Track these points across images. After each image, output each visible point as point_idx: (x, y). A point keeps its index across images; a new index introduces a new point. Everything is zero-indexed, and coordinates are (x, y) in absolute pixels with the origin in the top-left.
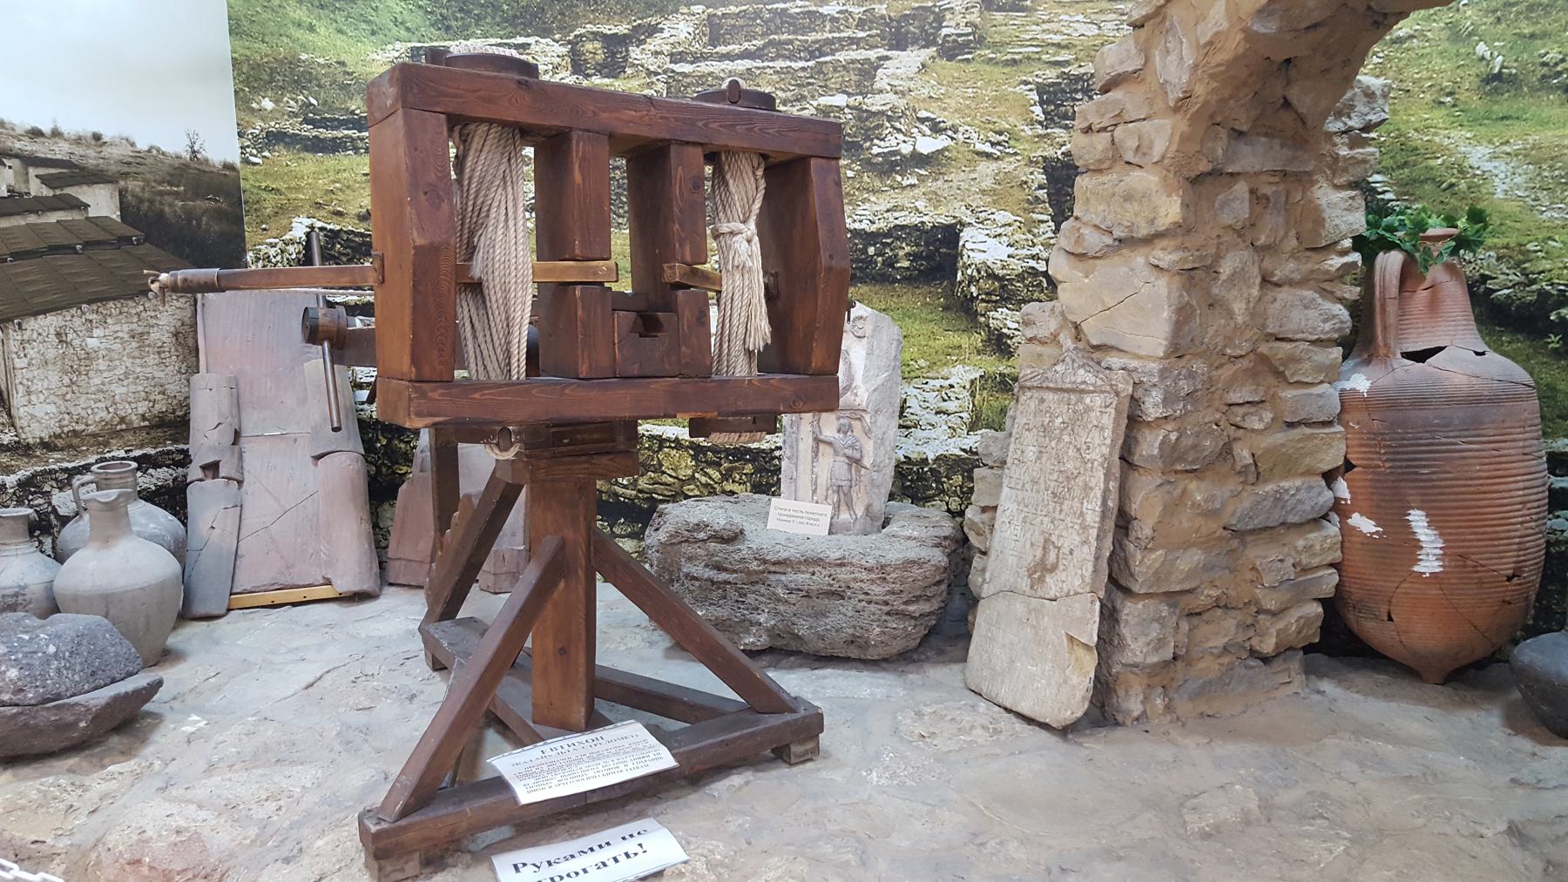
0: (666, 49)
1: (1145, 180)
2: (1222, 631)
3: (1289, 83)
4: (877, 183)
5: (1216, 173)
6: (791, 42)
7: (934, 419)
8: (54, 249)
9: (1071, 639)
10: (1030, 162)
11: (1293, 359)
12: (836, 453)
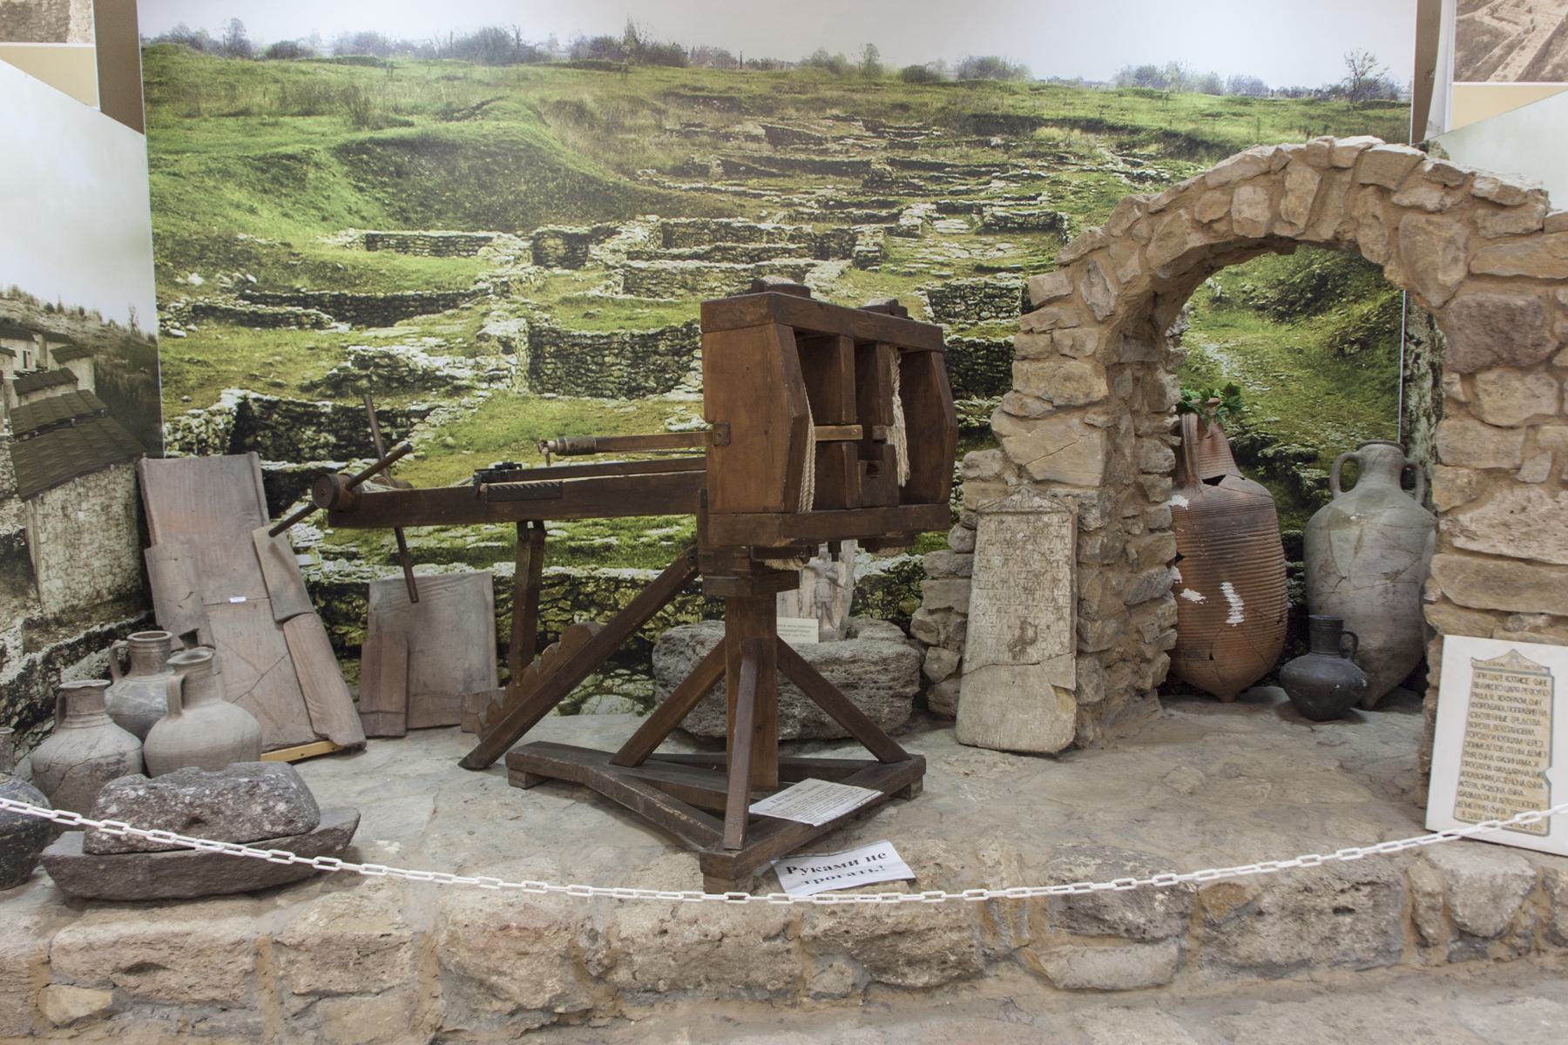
0: (624, 248)
2: (1125, 677)
6: (734, 249)
8: (63, 422)
9: (1055, 688)
11: (1153, 486)
12: (818, 575)
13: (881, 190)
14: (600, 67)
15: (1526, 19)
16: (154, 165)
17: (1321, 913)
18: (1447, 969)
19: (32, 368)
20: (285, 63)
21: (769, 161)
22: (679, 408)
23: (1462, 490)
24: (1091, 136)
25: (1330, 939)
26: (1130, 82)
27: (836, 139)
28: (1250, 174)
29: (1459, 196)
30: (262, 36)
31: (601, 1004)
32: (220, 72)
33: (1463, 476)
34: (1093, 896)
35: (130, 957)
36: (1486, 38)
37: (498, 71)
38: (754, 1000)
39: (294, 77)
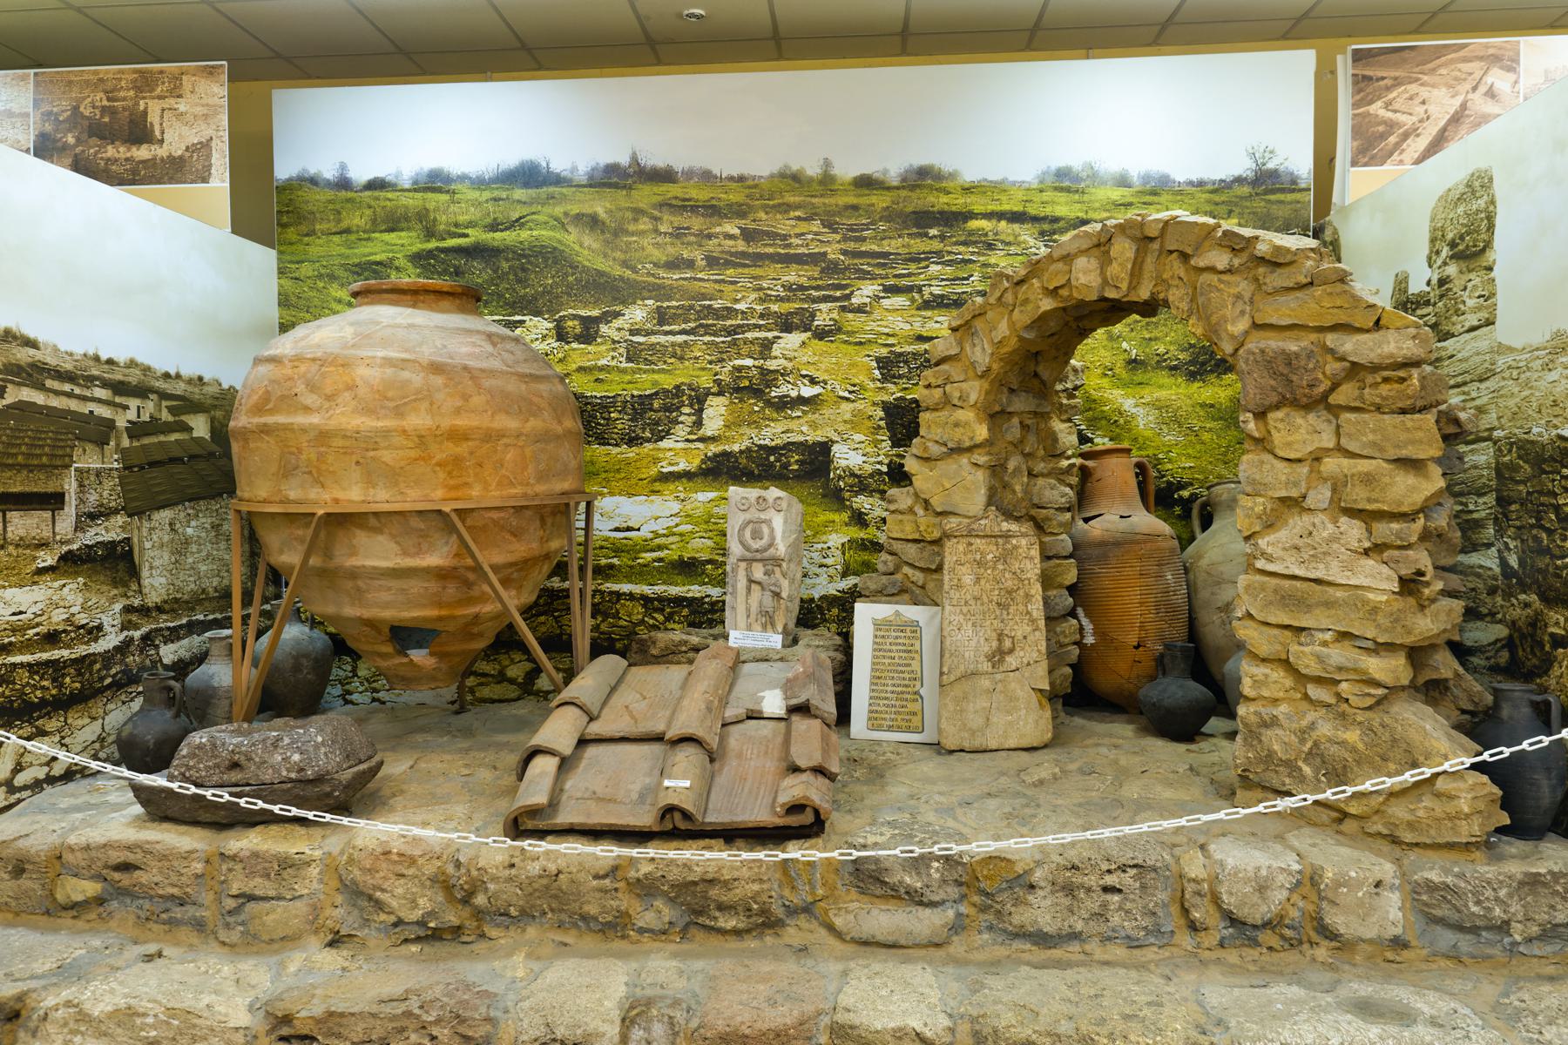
0: (627, 326)
1: (966, 415)
3: (1037, 363)
4: (775, 415)
5: (1003, 412)
7: (818, 571)
8: (173, 460)
10: (874, 404)
11: (1048, 519)
13: (835, 277)
14: (610, 185)
15: (1420, 110)
16: (281, 272)
17: (1089, 890)
18: (1220, 953)
19: (146, 417)
20: (376, 193)
21: (743, 254)
22: (669, 454)
23: (1259, 517)
24: (1016, 226)
25: (1101, 915)
26: (1049, 180)
27: (798, 236)
28: (1085, 247)
29: (1244, 257)
30: (360, 174)
31: (467, 923)
32: (330, 202)
33: (1259, 505)
34: (877, 860)
35: (117, 857)
36: (1381, 128)
37: (532, 192)
38: (590, 930)
39: (382, 203)
